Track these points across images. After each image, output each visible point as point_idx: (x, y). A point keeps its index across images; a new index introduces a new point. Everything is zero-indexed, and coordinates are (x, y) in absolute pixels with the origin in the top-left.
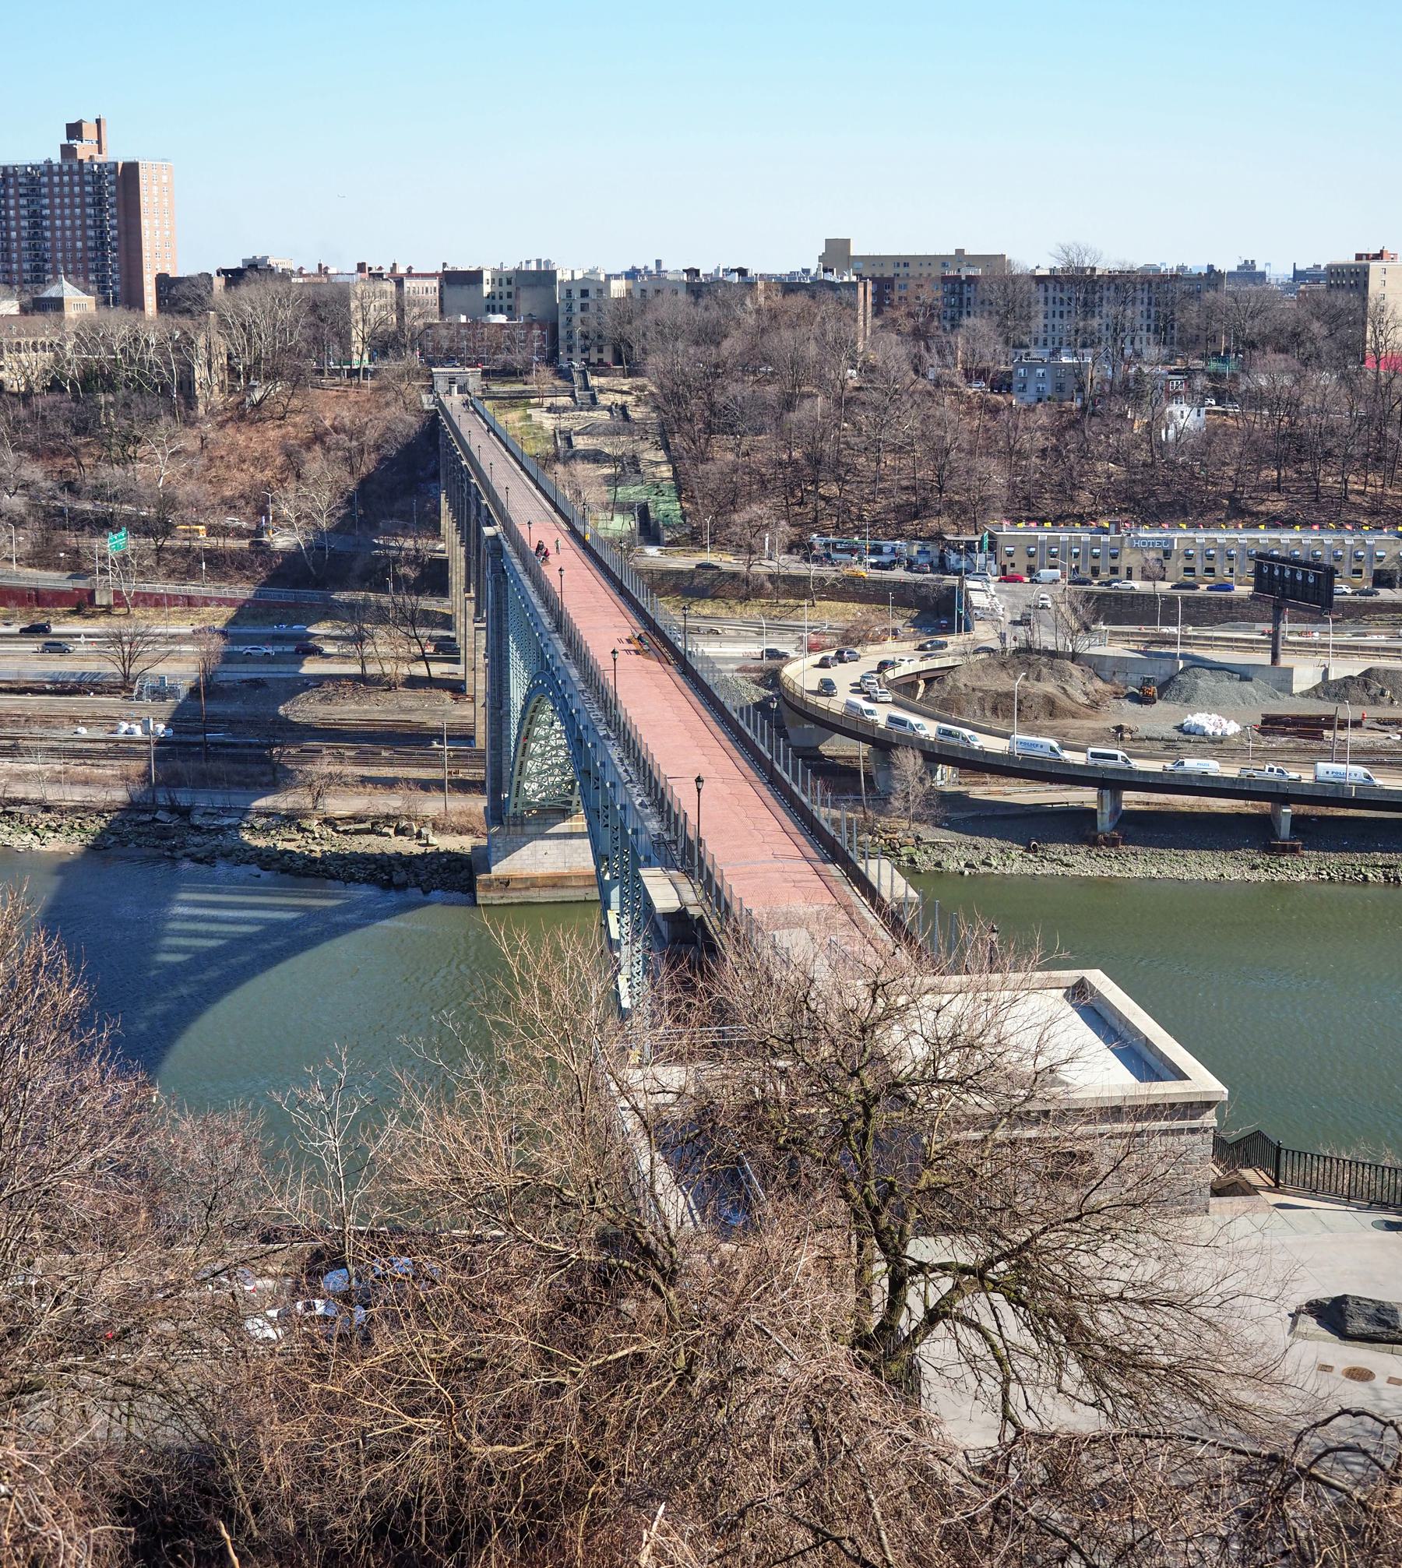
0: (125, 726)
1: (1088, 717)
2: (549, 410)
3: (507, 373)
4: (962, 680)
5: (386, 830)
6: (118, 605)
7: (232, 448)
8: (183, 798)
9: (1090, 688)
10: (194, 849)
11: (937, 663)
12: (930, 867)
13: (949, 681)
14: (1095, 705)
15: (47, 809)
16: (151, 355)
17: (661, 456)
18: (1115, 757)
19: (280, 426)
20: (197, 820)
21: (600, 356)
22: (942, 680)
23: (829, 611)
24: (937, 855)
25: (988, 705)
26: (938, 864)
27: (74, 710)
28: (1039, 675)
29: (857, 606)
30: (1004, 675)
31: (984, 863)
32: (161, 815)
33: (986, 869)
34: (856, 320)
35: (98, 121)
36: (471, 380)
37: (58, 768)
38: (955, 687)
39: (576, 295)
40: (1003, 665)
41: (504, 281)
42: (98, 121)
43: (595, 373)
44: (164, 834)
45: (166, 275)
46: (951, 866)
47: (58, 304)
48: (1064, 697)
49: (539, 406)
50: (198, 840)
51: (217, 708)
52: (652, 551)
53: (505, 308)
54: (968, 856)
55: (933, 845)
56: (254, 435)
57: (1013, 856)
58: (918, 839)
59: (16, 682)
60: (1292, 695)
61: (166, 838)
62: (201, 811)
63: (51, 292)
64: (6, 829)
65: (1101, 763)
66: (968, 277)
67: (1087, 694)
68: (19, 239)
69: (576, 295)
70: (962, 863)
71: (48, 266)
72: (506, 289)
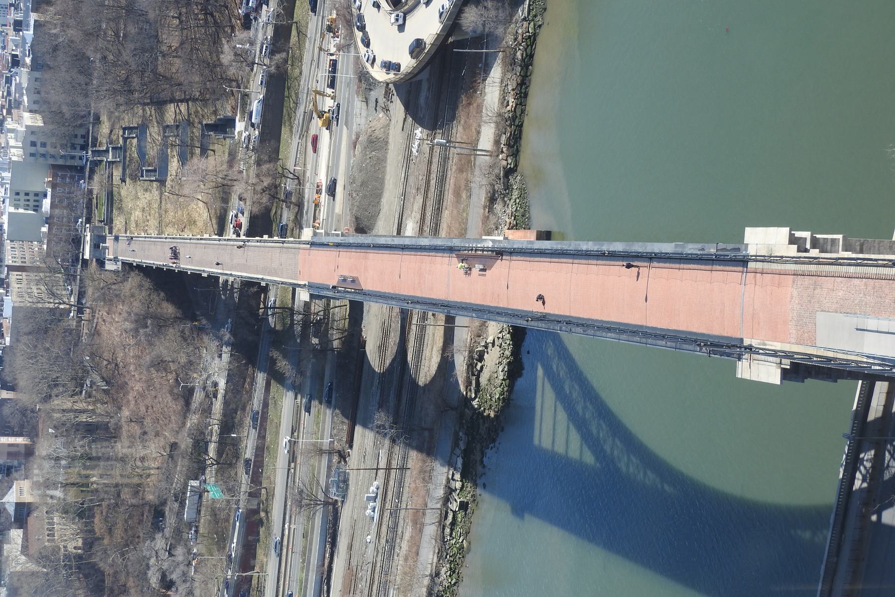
5: (478, 368)
21: (79, 136)
41: (17, 197)
47: (20, 506)
60: (338, 106)
63: (11, 510)
72: (22, 197)
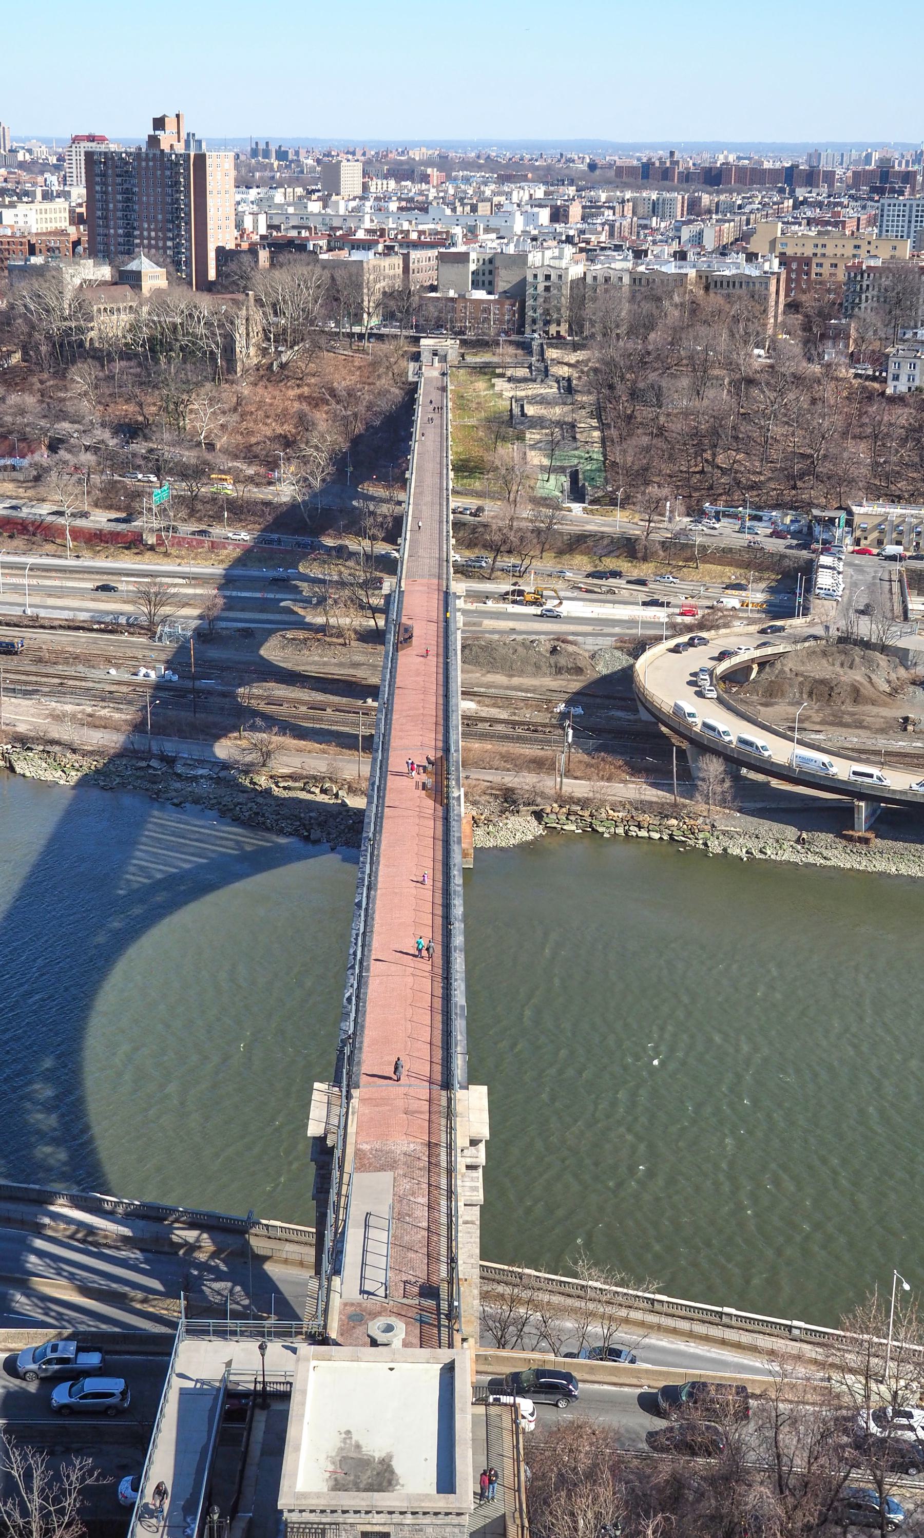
0: (143, 671)
1: (885, 705)
2: (510, 380)
3: (481, 344)
4: (790, 664)
5: (313, 789)
6: (158, 545)
7: (261, 404)
8: (170, 747)
9: (893, 676)
10: (174, 794)
11: (769, 651)
12: (719, 850)
13: (778, 665)
14: (894, 692)
15: (74, 751)
16: (201, 330)
17: (594, 422)
18: (871, 776)
19: (298, 386)
20: (180, 769)
22: (772, 664)
23: (709, 573)
24: (726, 842)
25: (806, 689)
26: (725, 850)
27: (111, 650)
28: (852, 663)
29: (733, 570)
30: (824, 661)
31: (761, 852)
32: (154, 763)
33: (762, 856)
34: (765, 311)
35: (178, 116)
36: (450, 351)
37: (89, 710)
38: (782, 671)
39: (541, 278)
40: (824, 654)
42: (178, 116)
43: (551, 345)
44: (154, 780)
45: (223, 248)
46: (735, 851)
48: (868, 685)
49: (502, 376)
50: (178, 785)
51: (214, 653)
52: (577, 508)
53: (486, 283)
54: (749, 845)
55: (724, 833)
56: (277, 393)
57: (785, 847)
58: (713, 826)
59: (73, 621)
61: (155, 783)
62: (182, 762)
63: (133, 266)
64: (44, 765)
65: (860, 779)
66: (868, 267)
67: (889, 682)
68: (116, 209)
69: (541, 278)
70: (744, 850)
71: (137, 233)
